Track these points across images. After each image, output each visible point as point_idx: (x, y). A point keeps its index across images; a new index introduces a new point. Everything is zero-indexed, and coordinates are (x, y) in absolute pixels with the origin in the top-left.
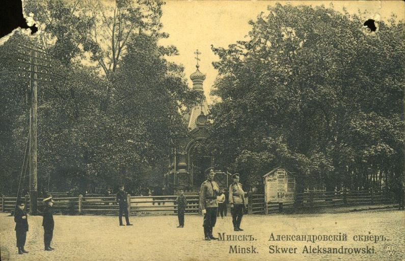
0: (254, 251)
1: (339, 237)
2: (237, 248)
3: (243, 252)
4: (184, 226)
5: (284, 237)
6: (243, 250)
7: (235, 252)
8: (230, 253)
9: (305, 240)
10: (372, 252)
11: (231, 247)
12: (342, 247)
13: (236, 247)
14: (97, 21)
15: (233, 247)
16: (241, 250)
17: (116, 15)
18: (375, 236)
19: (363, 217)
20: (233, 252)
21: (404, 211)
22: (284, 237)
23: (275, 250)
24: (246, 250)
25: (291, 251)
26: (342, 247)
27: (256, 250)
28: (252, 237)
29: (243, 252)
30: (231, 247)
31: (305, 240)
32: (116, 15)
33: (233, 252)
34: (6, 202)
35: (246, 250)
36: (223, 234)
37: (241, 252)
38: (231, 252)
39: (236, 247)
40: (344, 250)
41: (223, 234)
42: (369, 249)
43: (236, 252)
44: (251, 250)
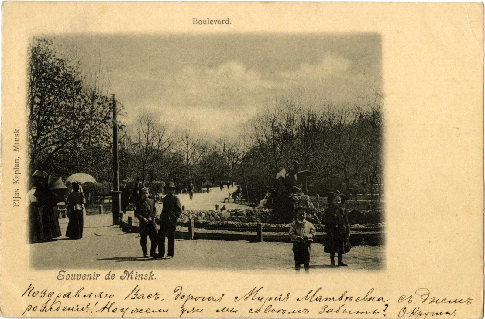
0: (18, 131)
2: (15, 145)
4: (174, 255)
7: (18, 147)
9: (18, 160)
11: (14, 150)
12: (20, 174)
13: (14, 146)
14: (204, 152)
15: (15, 148)
19: (285, 245)
20: (18, 149)
23: (17, 137)
24: (18, 137)
26: (20, 174)
27: (17, 130)
31: (18, 160)
33: (18, 149)
34: (255, 234)
35: (18, 137)
38: (18, 150)
39: (14, 146)
40: (18, 175)
42: (16, 131)
44: (17, 133)
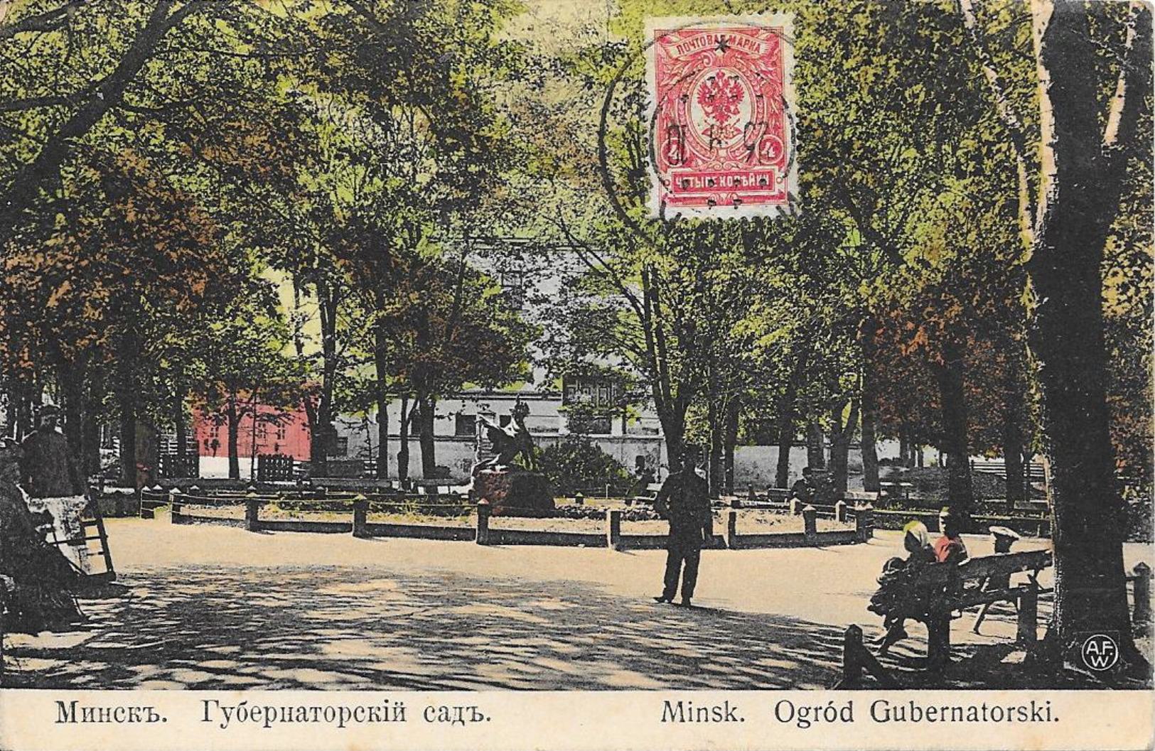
1: (383, 710)
2: (686, 706)
3: (703, 718)
5: (256, 710)
6: (899, 716)
7: (678, 717)
8: (664, 720)
10: (1045, 717)
11: (668, 703)
13: (680, 704)
16: (695, 713)
17: (408, 411)
18: (267, 709)
21: (1150, 695)
22: (256, 710)
24: (711, 715)
25: (932, 716)
28: (153, 711)
29: (703, 718)
30: (668, 703)
32: (408, 411)
33: (673, 717)
35: (711, 715)
36: (73, 704)
37: (695, 717)
38: (668, 717)
41: (73, 704)
43: (683, 721)
